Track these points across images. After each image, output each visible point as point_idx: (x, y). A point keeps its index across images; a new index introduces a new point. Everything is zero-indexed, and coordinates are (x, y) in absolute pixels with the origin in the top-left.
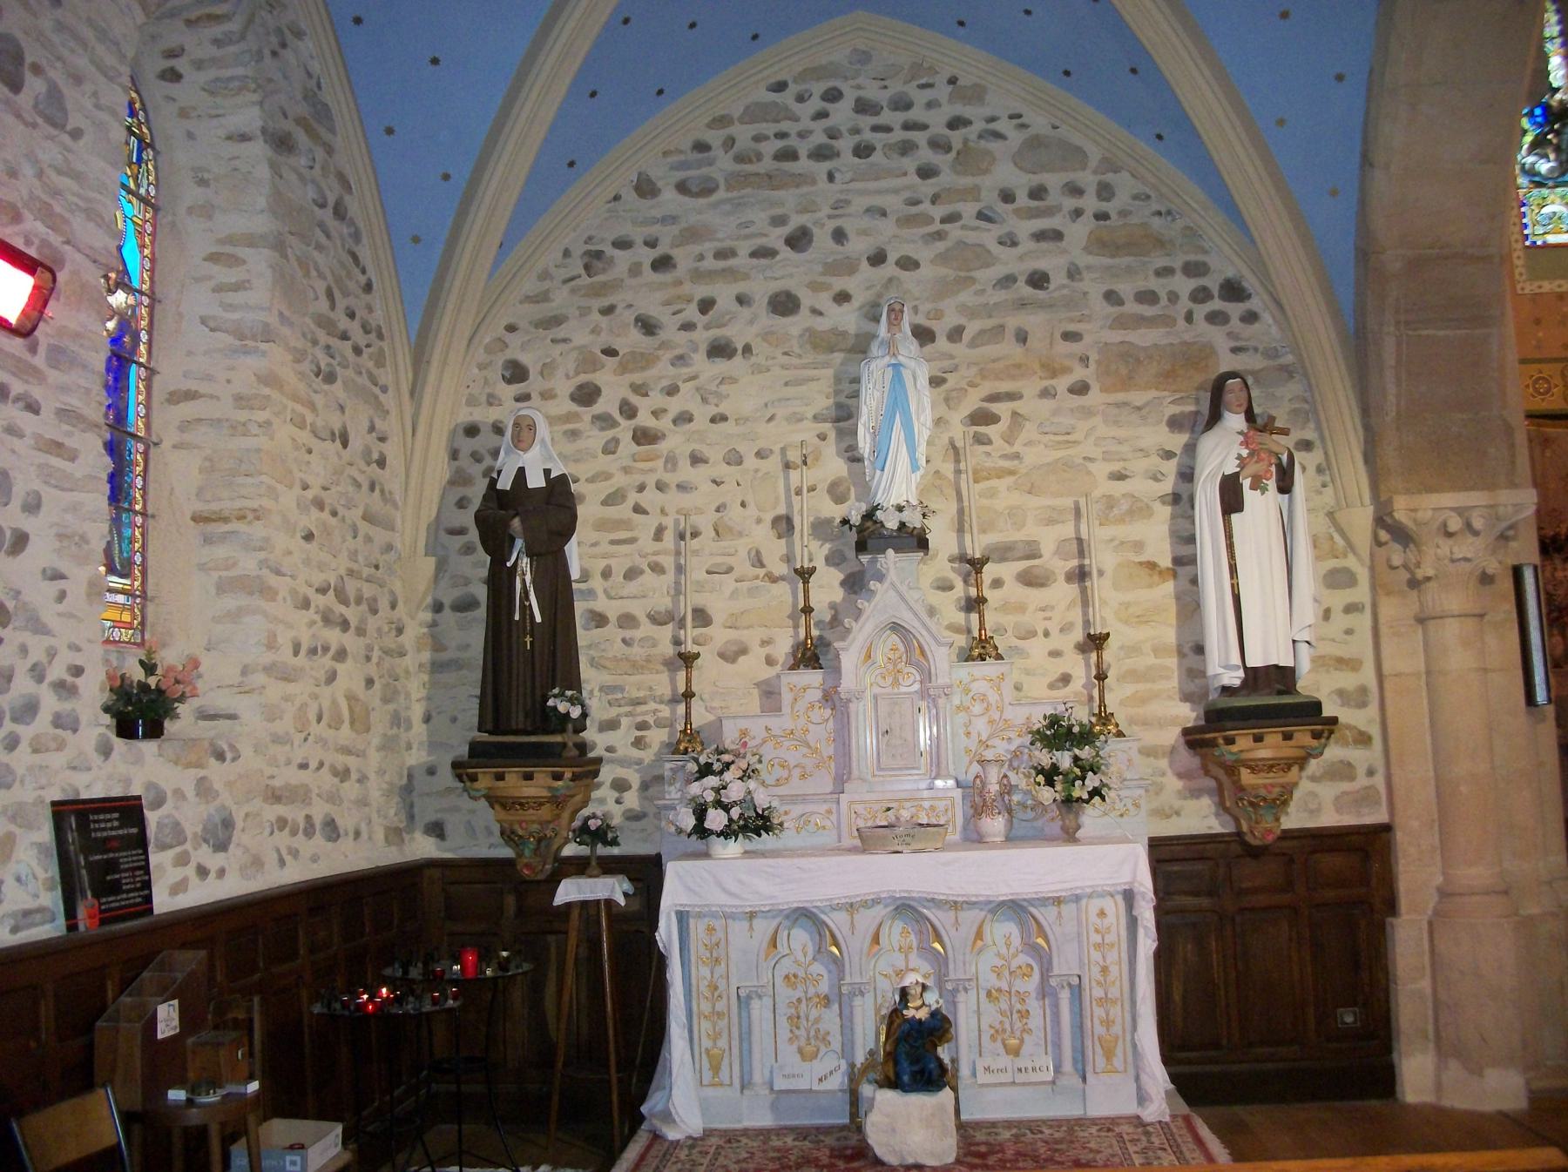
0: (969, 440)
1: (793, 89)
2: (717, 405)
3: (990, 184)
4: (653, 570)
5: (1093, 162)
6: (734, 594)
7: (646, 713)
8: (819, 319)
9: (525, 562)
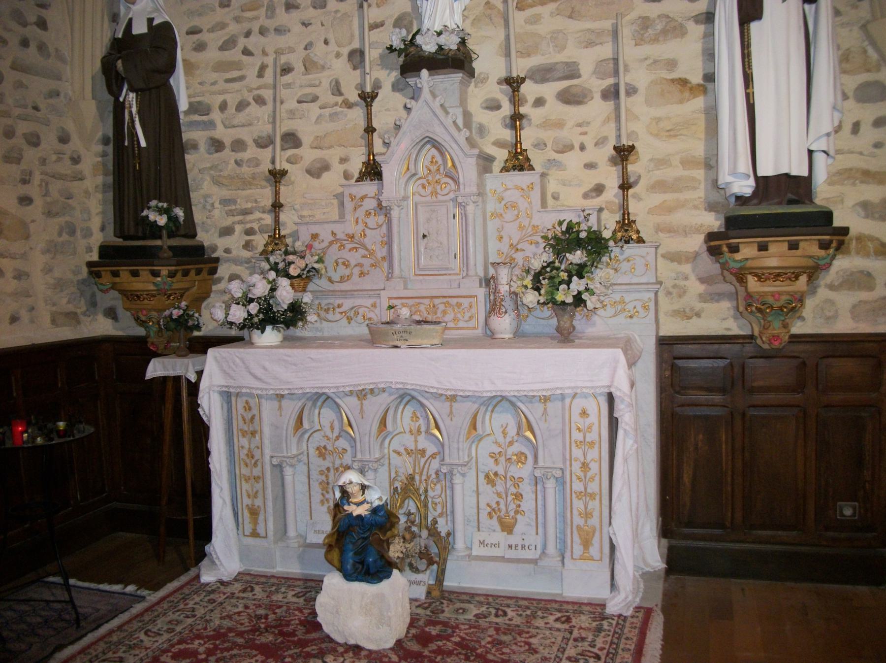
6: (319, 119)
7: (251, 222)
9: (132, 96)
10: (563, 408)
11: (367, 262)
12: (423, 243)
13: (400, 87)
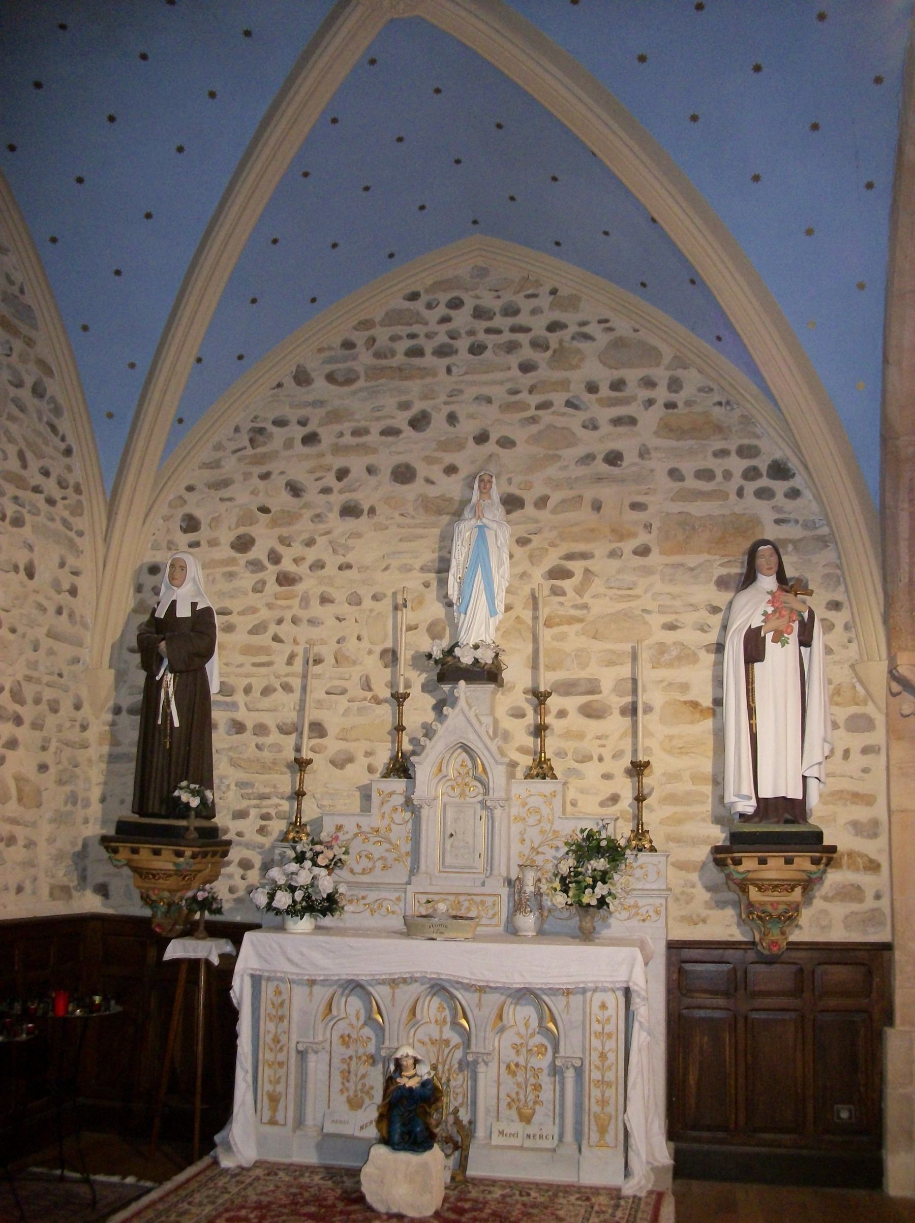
0: (546, 592)
1: (424, 298)
2: (344, 556)
3: (578, 377)
4: (283, 688)
5: (666, 361)
6: (346, 713)
8: (431, 487)
9: (170, 677)
10: (584, 1001)
11: (390, 856)
12: (449, 842)
13: (430, 688)
